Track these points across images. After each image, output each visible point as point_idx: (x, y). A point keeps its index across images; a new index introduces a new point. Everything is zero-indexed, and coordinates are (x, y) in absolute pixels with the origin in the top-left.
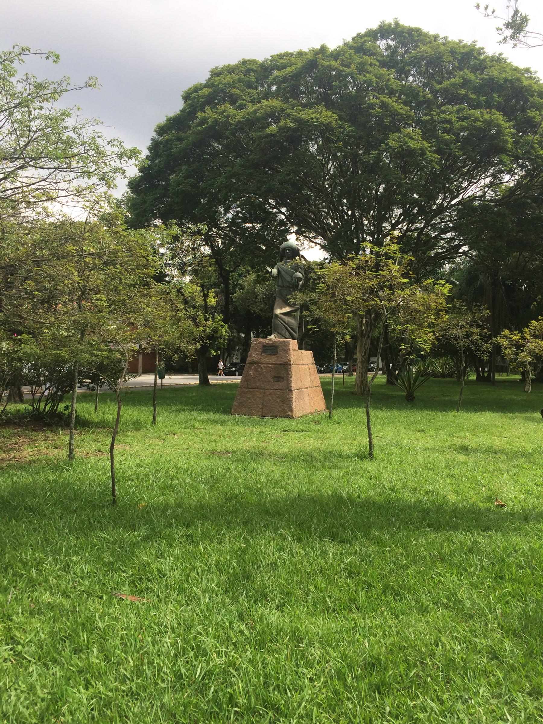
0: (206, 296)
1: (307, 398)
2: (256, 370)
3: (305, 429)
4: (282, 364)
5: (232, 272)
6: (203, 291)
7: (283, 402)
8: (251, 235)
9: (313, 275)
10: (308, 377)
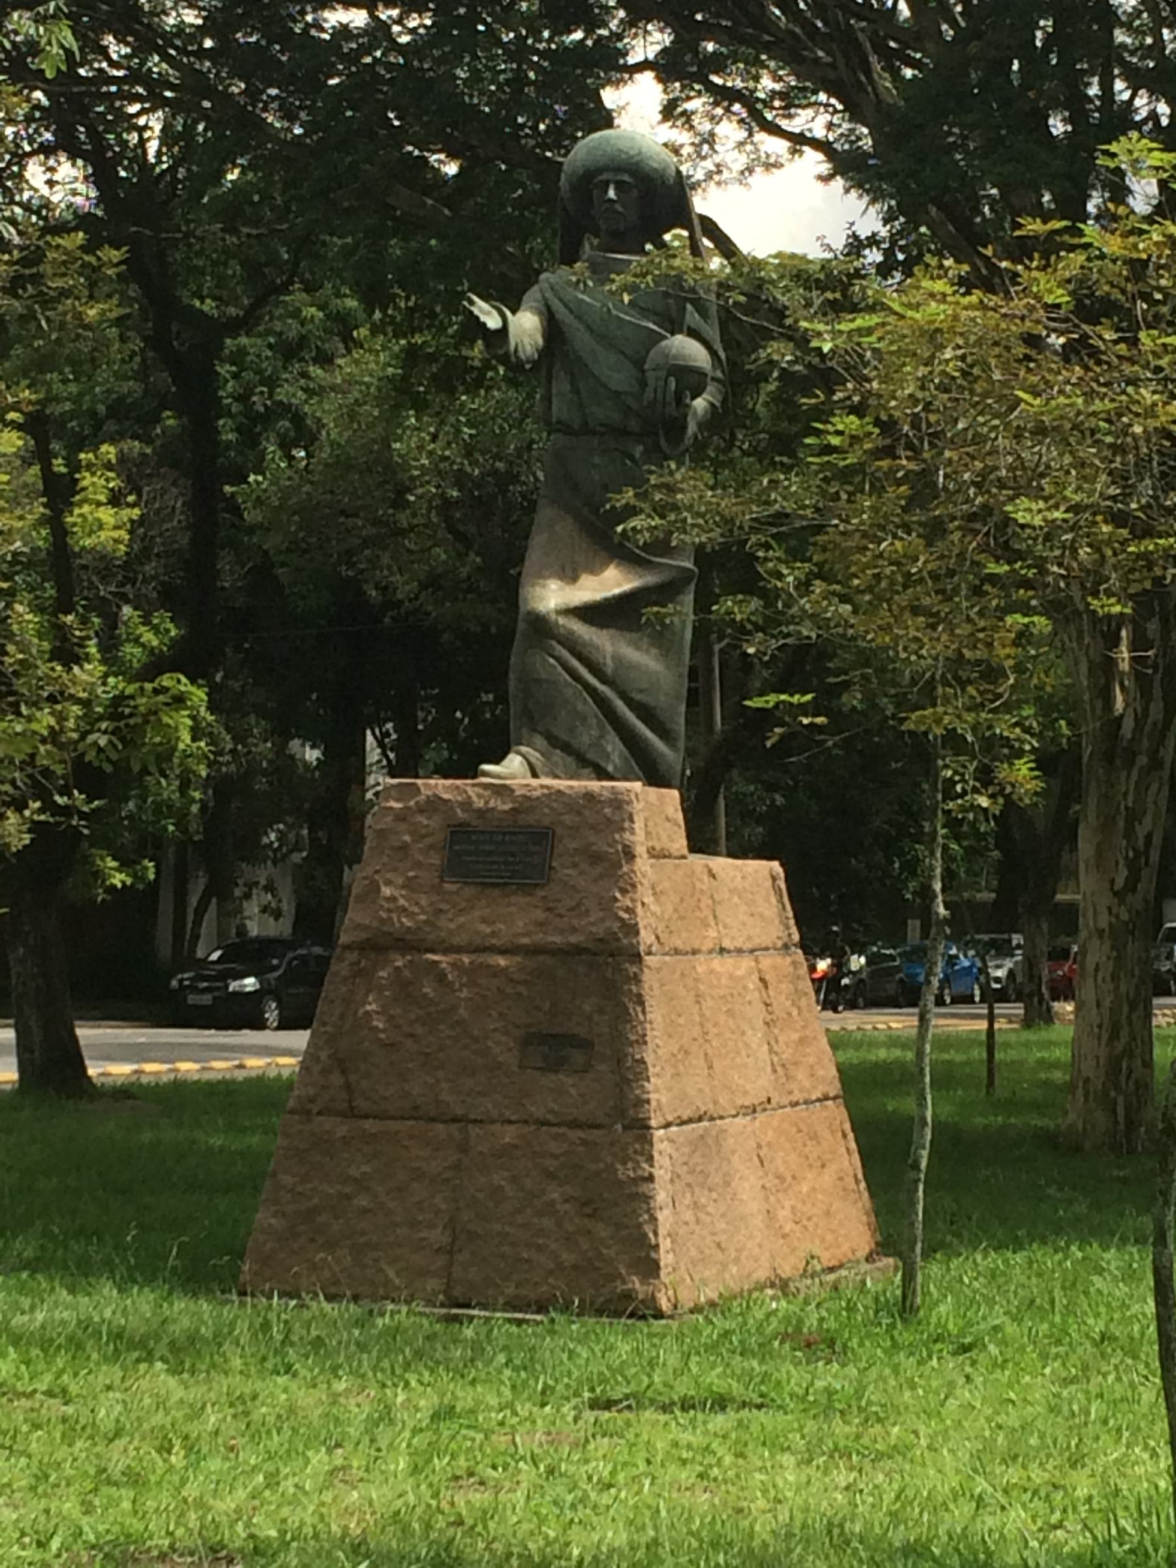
0: (60, 493)
1: (748, 1185)
2: (404, 989)
3: (737, 1389)
4: (578, 950)
5: (235, 327)
6: (42, 455)
7: (590, 1207)
8: (364, 84)
9: (781, 353)
10: (756, 1038)
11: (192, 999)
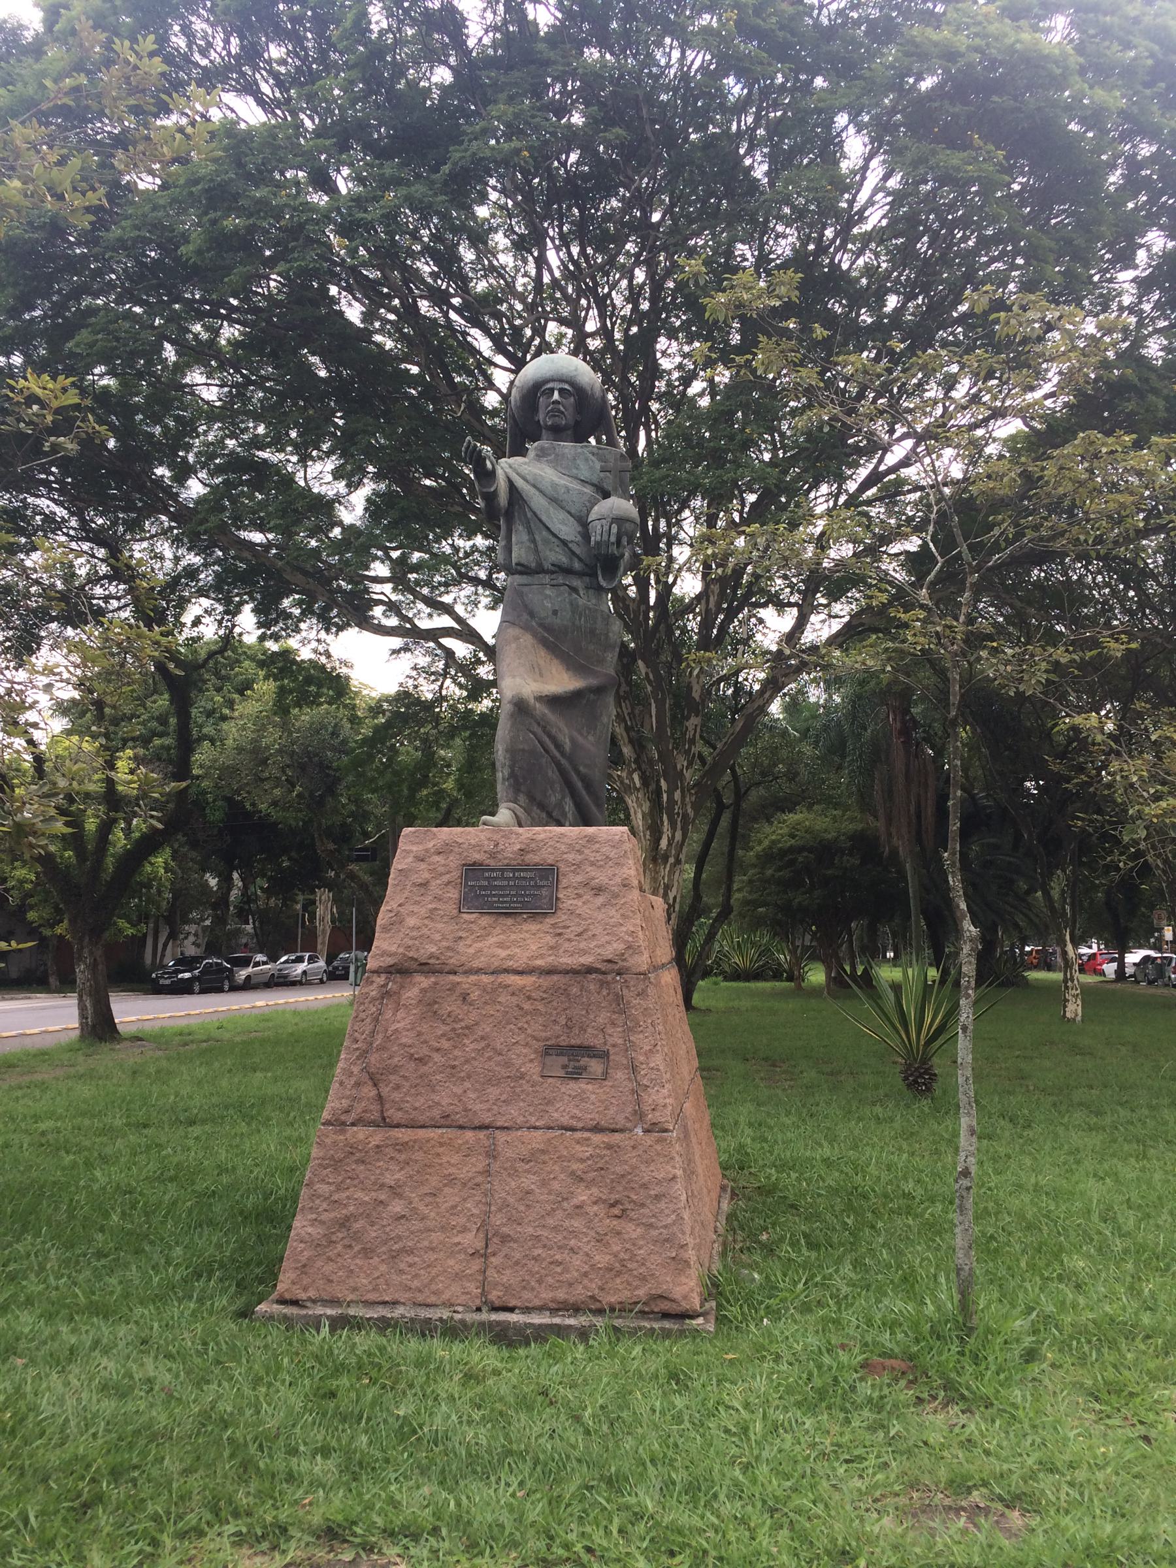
2: (430, 1006)
4: (590, 970)
7: (619, 1209)
11: (162, 982)
